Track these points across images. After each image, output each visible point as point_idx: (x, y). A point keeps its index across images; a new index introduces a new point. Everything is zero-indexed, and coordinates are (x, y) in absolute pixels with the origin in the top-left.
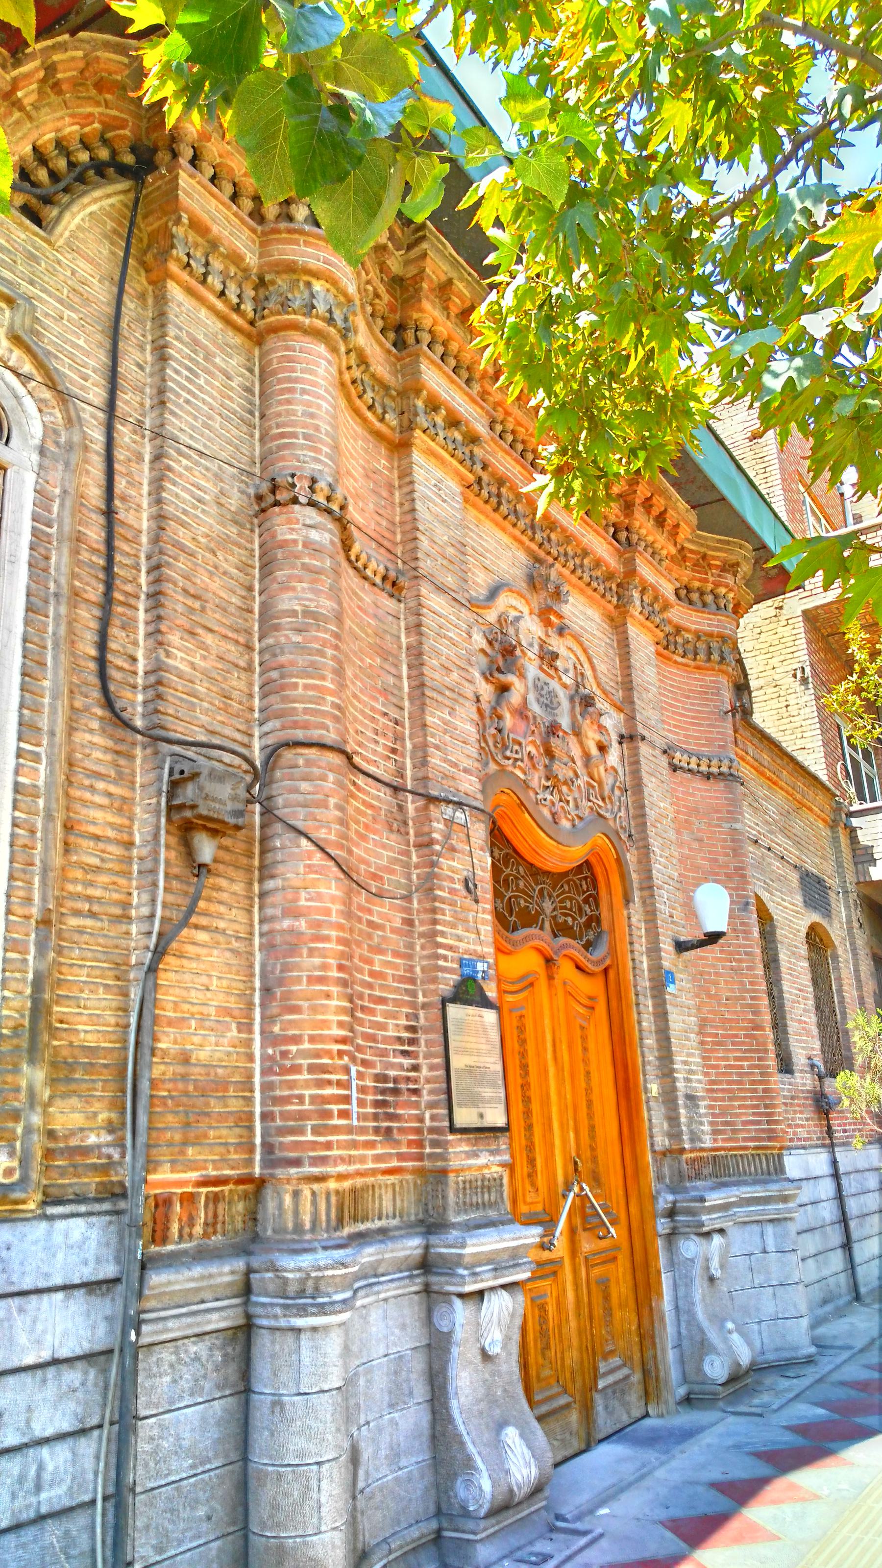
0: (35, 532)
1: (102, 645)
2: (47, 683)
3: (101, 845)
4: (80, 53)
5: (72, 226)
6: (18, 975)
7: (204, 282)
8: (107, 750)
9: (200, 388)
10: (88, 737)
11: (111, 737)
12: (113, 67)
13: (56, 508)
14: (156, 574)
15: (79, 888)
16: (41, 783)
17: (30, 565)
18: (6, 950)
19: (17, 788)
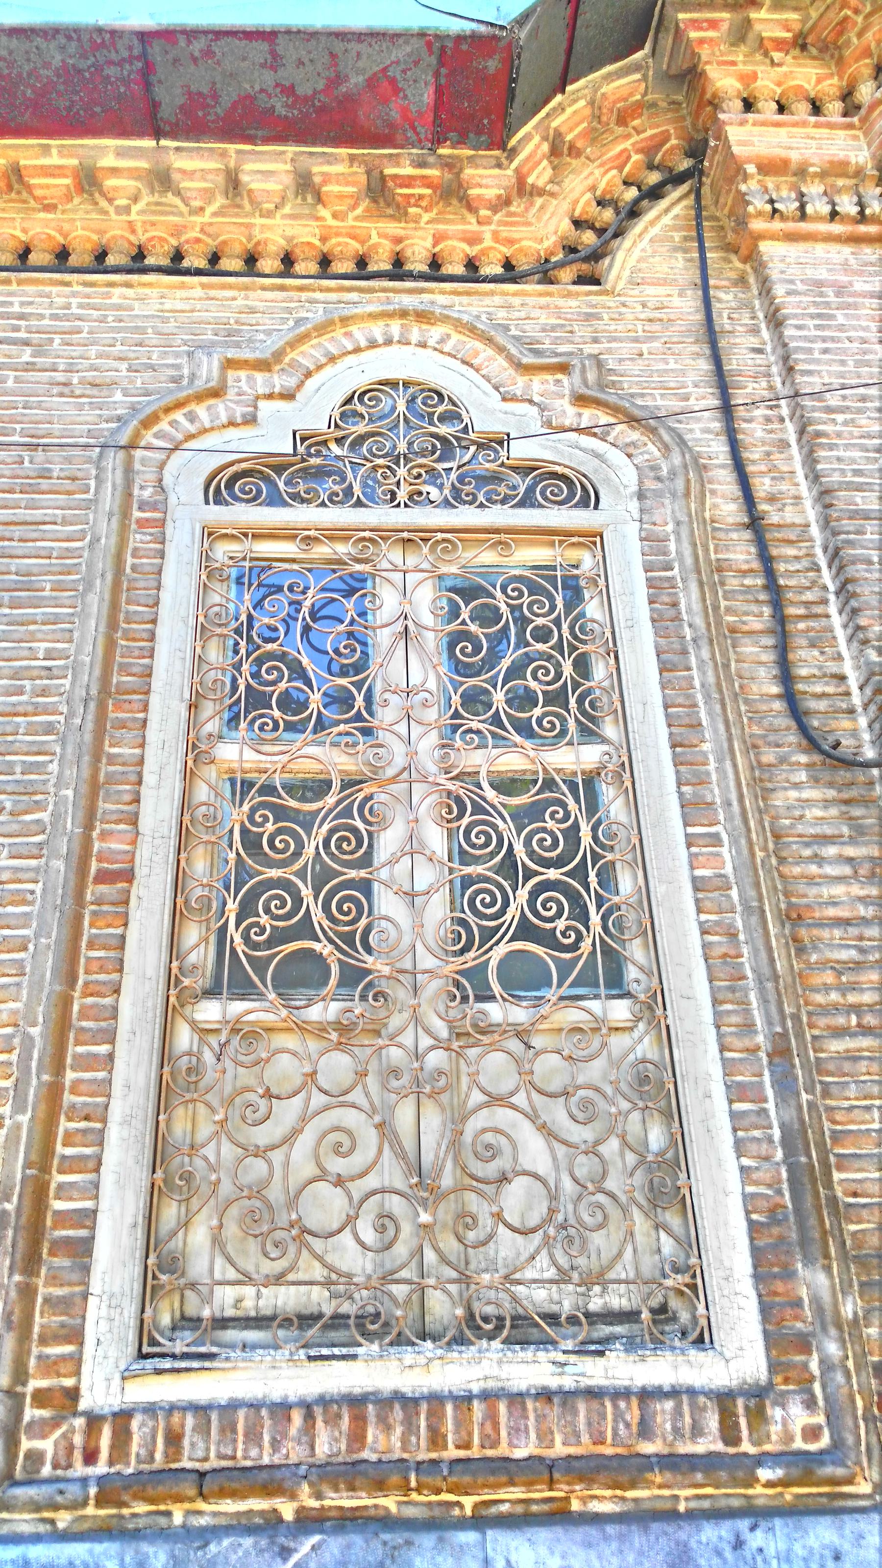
0: (651, 584)
1: (786, 675)
2: (706, 747)
3: (853, 931)
4: (582, 103)
5: (632, 262)
6: (757, 1133)
7: (803, 216)
8: (827, 803)
9: (841, 328)
10: (793, 794)
11: (831, 785)
12: (624, 92)
13: (672, 546)
14: (837, 562)
15: (834, 996)
16: (729, 869)
17: (653, 621)
18: (731, 1102)
19: (698, 885)
